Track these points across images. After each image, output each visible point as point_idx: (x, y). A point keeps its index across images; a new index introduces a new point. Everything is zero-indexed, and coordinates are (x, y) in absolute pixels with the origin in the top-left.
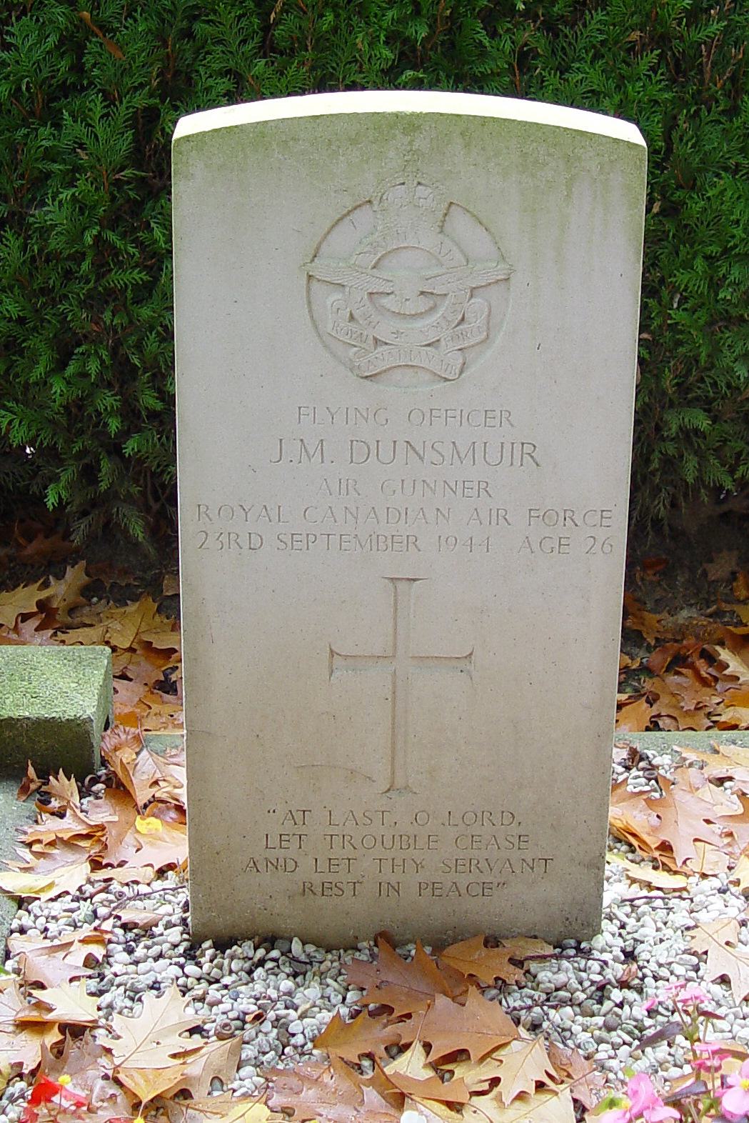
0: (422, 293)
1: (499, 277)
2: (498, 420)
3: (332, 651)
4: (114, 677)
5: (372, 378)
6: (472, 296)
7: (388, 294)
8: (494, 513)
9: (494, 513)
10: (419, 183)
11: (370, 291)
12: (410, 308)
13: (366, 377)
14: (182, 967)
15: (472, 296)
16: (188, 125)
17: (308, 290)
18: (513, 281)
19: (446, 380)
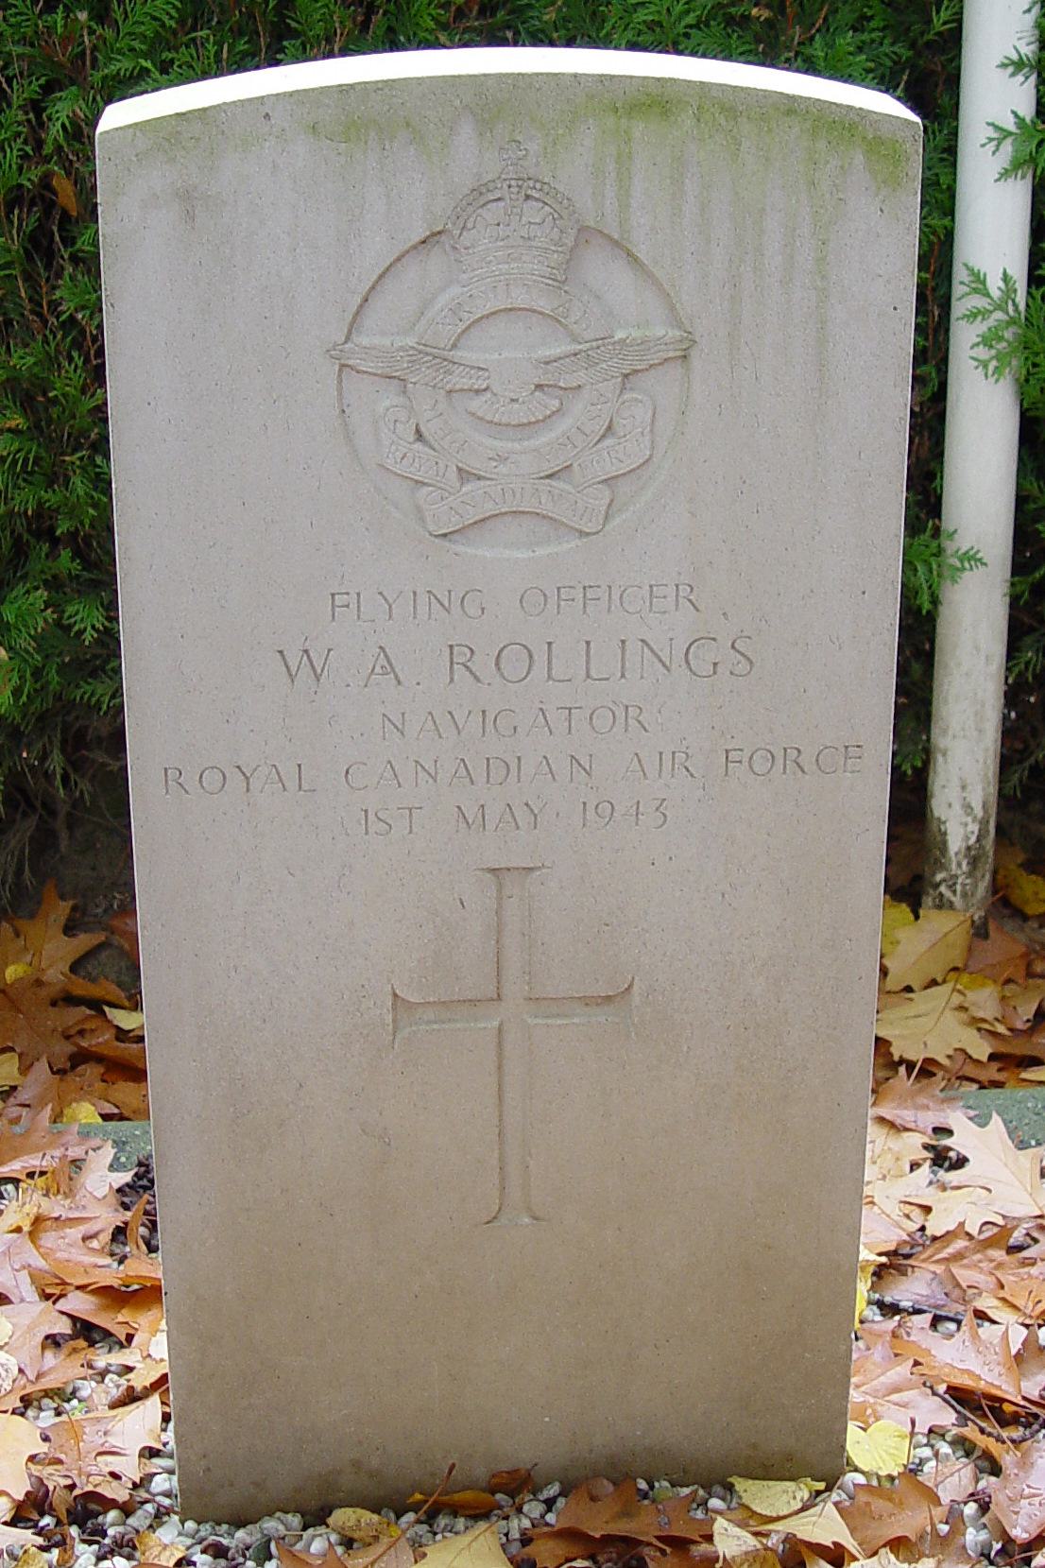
0: (539, 387)
1: (671, 354)
2: (672, 599)
3: (395, 995)
4: (113, 1406)
5: (455, 537)
6: (623, 389)
7: (477, 392)
8: (667, 757)
9: (667, 757)
10: (528, 197)
11: (448, 387)
12: (520, 414)
13: (445, 535)
14: (1000, 307)
15: (623, 389)
16: (116, 116)
17: (340, 382)
18: (696, 361)
19: (582, 534)
